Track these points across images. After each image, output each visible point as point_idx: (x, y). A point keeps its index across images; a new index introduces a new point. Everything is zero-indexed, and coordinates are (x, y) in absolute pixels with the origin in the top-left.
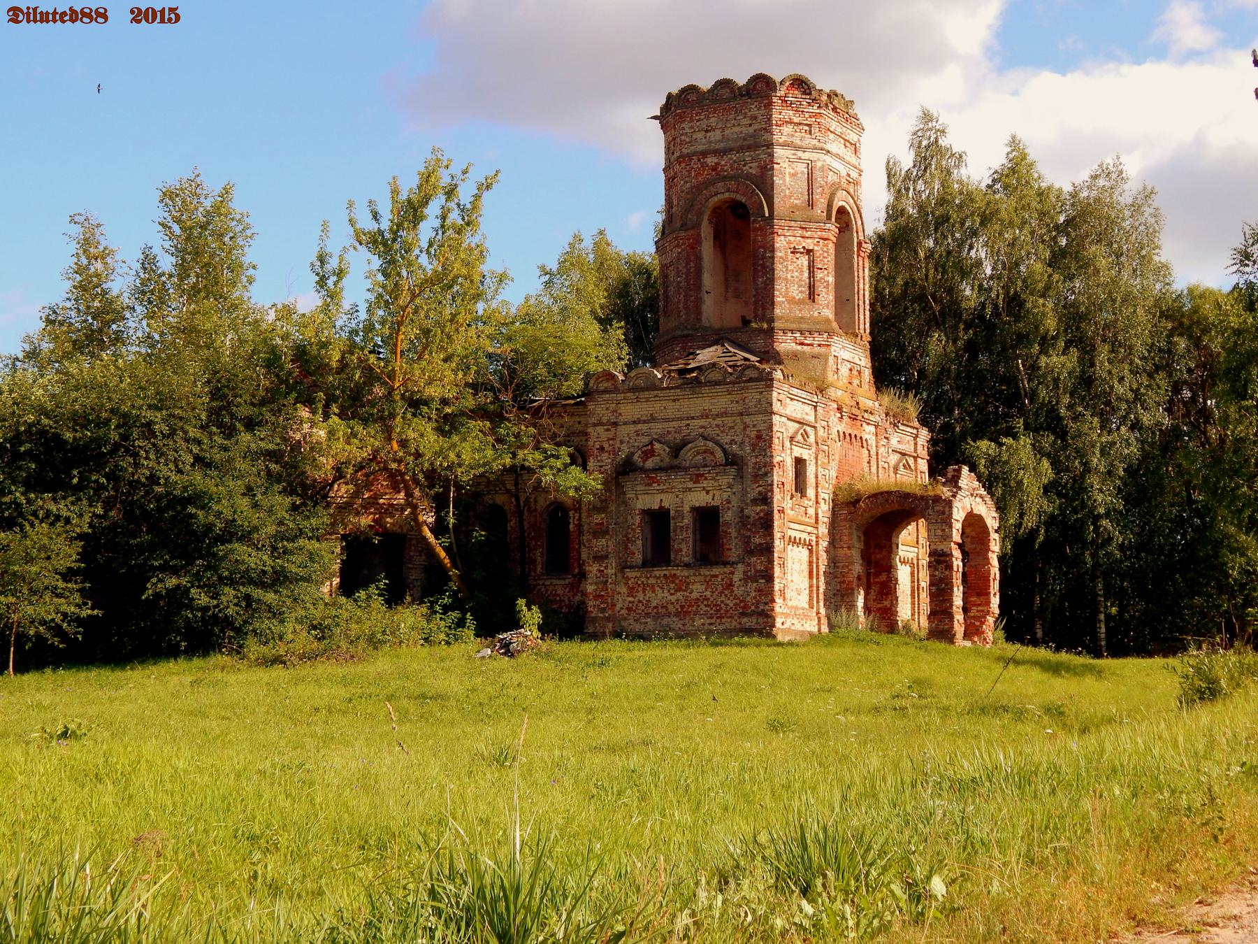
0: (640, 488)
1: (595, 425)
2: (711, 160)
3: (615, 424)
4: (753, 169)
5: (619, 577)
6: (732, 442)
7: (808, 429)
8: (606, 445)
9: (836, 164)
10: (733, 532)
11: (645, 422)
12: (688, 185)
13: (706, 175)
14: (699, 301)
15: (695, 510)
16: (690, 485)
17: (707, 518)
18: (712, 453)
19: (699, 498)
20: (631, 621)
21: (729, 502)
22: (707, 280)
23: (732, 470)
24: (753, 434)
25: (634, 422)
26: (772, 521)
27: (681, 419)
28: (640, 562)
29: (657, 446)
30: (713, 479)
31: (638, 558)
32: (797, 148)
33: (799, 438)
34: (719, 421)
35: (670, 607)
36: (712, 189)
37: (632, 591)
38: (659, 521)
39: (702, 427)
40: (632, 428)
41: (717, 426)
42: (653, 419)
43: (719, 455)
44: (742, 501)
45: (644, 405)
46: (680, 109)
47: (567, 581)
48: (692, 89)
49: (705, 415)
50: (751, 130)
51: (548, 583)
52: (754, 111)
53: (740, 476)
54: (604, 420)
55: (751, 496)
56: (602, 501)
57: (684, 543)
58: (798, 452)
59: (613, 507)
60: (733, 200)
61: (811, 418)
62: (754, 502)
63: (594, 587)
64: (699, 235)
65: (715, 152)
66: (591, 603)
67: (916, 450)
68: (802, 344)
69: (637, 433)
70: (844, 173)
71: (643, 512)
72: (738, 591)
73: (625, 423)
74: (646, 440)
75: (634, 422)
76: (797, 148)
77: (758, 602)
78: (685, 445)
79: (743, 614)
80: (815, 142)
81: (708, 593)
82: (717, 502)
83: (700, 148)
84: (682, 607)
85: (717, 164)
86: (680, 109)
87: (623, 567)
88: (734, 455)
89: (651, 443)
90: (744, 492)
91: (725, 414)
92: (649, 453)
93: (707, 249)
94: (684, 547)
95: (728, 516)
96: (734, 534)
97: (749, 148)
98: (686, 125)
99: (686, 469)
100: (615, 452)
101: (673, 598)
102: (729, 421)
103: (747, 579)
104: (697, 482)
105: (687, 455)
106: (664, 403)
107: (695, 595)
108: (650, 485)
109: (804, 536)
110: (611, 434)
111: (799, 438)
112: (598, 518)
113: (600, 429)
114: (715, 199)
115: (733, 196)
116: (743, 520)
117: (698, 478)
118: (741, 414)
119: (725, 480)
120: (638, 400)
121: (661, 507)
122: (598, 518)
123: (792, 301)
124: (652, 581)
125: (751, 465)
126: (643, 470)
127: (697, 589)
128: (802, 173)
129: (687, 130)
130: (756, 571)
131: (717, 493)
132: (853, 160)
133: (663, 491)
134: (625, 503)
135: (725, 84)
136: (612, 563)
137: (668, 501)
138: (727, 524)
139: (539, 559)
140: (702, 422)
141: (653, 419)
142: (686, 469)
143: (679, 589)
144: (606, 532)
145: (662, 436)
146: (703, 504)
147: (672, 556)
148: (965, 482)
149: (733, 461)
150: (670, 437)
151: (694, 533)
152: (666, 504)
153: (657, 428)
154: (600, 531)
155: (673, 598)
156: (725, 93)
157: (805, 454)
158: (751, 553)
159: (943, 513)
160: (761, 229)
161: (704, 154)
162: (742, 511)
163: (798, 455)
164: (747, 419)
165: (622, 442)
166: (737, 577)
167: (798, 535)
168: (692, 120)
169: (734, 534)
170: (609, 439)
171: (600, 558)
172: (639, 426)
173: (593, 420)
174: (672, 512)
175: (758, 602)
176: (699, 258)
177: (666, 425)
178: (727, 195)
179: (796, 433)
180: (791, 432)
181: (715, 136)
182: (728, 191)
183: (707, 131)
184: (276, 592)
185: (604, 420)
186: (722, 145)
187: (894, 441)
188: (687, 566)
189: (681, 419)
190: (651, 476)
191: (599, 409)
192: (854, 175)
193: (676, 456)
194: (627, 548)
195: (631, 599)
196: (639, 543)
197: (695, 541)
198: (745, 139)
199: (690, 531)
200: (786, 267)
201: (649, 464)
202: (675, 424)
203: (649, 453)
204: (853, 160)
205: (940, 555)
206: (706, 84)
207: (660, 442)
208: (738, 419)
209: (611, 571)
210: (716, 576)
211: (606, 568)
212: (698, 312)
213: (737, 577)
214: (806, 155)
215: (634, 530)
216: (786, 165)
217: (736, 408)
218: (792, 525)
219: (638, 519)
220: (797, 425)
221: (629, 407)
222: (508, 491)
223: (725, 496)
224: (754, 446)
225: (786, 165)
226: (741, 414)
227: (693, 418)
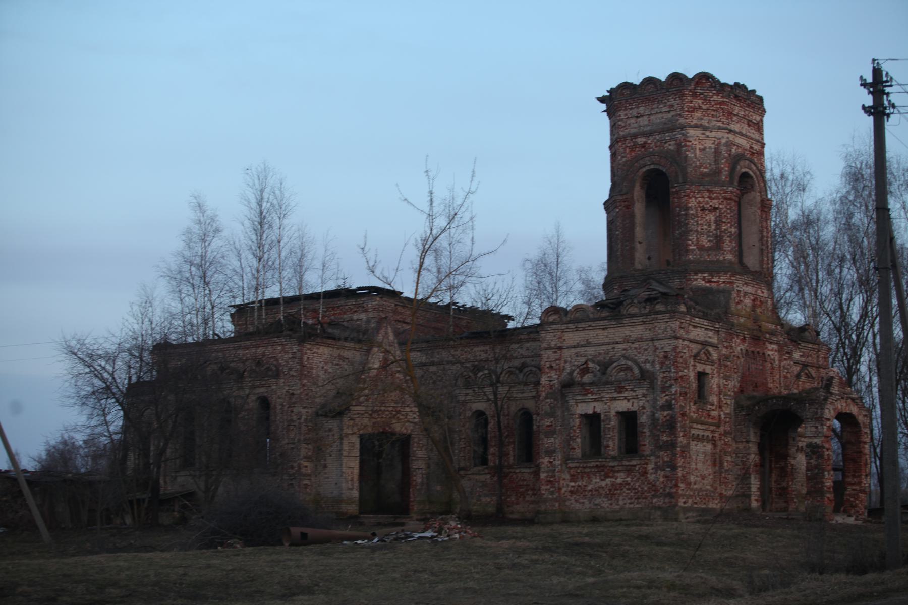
1: (546, 349)
2: (641, 140)
3: (560, 348)
5: (564, 467)
6: (646, 361)
7: (710, 349)
8: (554, 365)
9: (741, 141)
11: (582, 346)
12: (624, 160)
13: (638, 151)
14: (632, 249)
15: (619, 414)
16: (615, 395)
17: (629, 419)
19: (623, 406)
20: (573, 501)
21: (644, 408)
22: (639, 232)
23: (646, 384)
24: (661, 355)
25: (574, 347)
27: (609, 344)
28: (580, 455)
31: (578, 452)
32: (705, 128)
34: (636, 345)
35: (601, 491)
36: (641, 162)
37: (573, 478)
38: (593, 421)
39: (624, 350)
40: (573, 351)
41: (635, 348)
42: (588, 344)
43: (636, 371)
44: (654, 407)
45: (582, 333)
46: (619, 100)
48: (625, 86)
49: (626, 340)
50: (669, 116)
51: (517, 471)
52: (672, 102)
53: (652, 387)
54: (553, 345)
56: (551, 408)
57: (612, 443)
58: (700, 367)
59: (559, 413)
60: (657, 170)
61: (715, 341)
62: (663, 408)
63: (545, 475)
64: (632, 197)
66: (543, 487)
67: (818, 361)
68: (710, 282)
70: (748, 146)
71: (582, 416)
72: (651, 478)
73: (568, 348)
74: (583, 360)
75: (574, 347)
76: (705, 128)
77: (665, 486)
80: (720, 124)
81: (629, 479)
83: (633, 131)
84: (610, 490)
85: (645, 143)
87: (567, 459)
89: (586, 363)
92: (585, 370)
93: (639, 209)
94: (611, 443)
95: (643, 419)
98: (622, 113)
99: (611, 383)
101: (603, 484)
102: (644, 345)
103: (657, 468)
104: (620, 392)
105: (614, 373)
106: (596, 332)
107: (619, 481)
108: (586, 395)
109: (706, 433)
110: (557, 356)
112: (547, 422)
113: (550, 352)
114: (644, 170)
116: (654, 420)
117: (620, 389)
118: (652, 340)
119: (640, 392)
121: (595, 413)
122: (547, 422)
123: (701, 248)
124: (588, 470)
125: (660, 379)
126: (582, 385)
127: (620, 478)
128: (710, 148)
129: (623, 117)
131: (635, 401)
133: (595, 400)
134: (568, 409)
135: (650, 81)
137: (599, 408)
138: (643, 425)
139: (511, 453)
140: (625, 346)
141: (588, 344)
142: (611, 383)
143: (607, 476)
146: (625, 410)
149: (645, 376)
150: (601, 358)
152: (598, 410)
153: (591, 351)
154: (551, 433)
155: (603, 484)
156: (651, 88)
157: (708, 369)
158: (660, 448)
159: (816, 413)
161: (635, 136)
163: (700, 370)
164: (657, 343)
165: (566, 362)
166: (650, 467)
167: (701, 433)
168: (626, 110)
169: (648, 433)
170: (557, 360)
171: (550, 453)
172: (578, 350)
173: (544, 345)
174: (602, 417)
175: (665, 486)
176: (632, 216)
177: (598, 348)
178: (652, 167)
179: (701, 350)
180: (695, 351)
181: (644, 121)
183: (637, 117)
186: (649, 128)
187: (797, 355)
188: (614, 458)
189: (609, 344)
190: (585, 389)
192: (756, 147)
193: (604, 373)
195: (573, 484)
196: (579, 440)
198: (665, 123)
199: (616, 431)
200: (697, 222)
201: (587, 378)
203: (585, 370)
204: (756, 136)
206: (636, 79)
207: (593, 362)
209: (558, 463)
210: (635, 466)
211: (554, 460)
212: (632, 259)
213: (650, 467)
214: (713, 134)
215: (575, 431)
216: (696, 142)
217: (648, 335)
219: (577, 421)
220: (700, 347)
221: (571, 334)
222: (489, 400)
223: (641, 403)
224: (662, 364)
225: (696, 142)
226: (652, 340)
227: (617, 343)
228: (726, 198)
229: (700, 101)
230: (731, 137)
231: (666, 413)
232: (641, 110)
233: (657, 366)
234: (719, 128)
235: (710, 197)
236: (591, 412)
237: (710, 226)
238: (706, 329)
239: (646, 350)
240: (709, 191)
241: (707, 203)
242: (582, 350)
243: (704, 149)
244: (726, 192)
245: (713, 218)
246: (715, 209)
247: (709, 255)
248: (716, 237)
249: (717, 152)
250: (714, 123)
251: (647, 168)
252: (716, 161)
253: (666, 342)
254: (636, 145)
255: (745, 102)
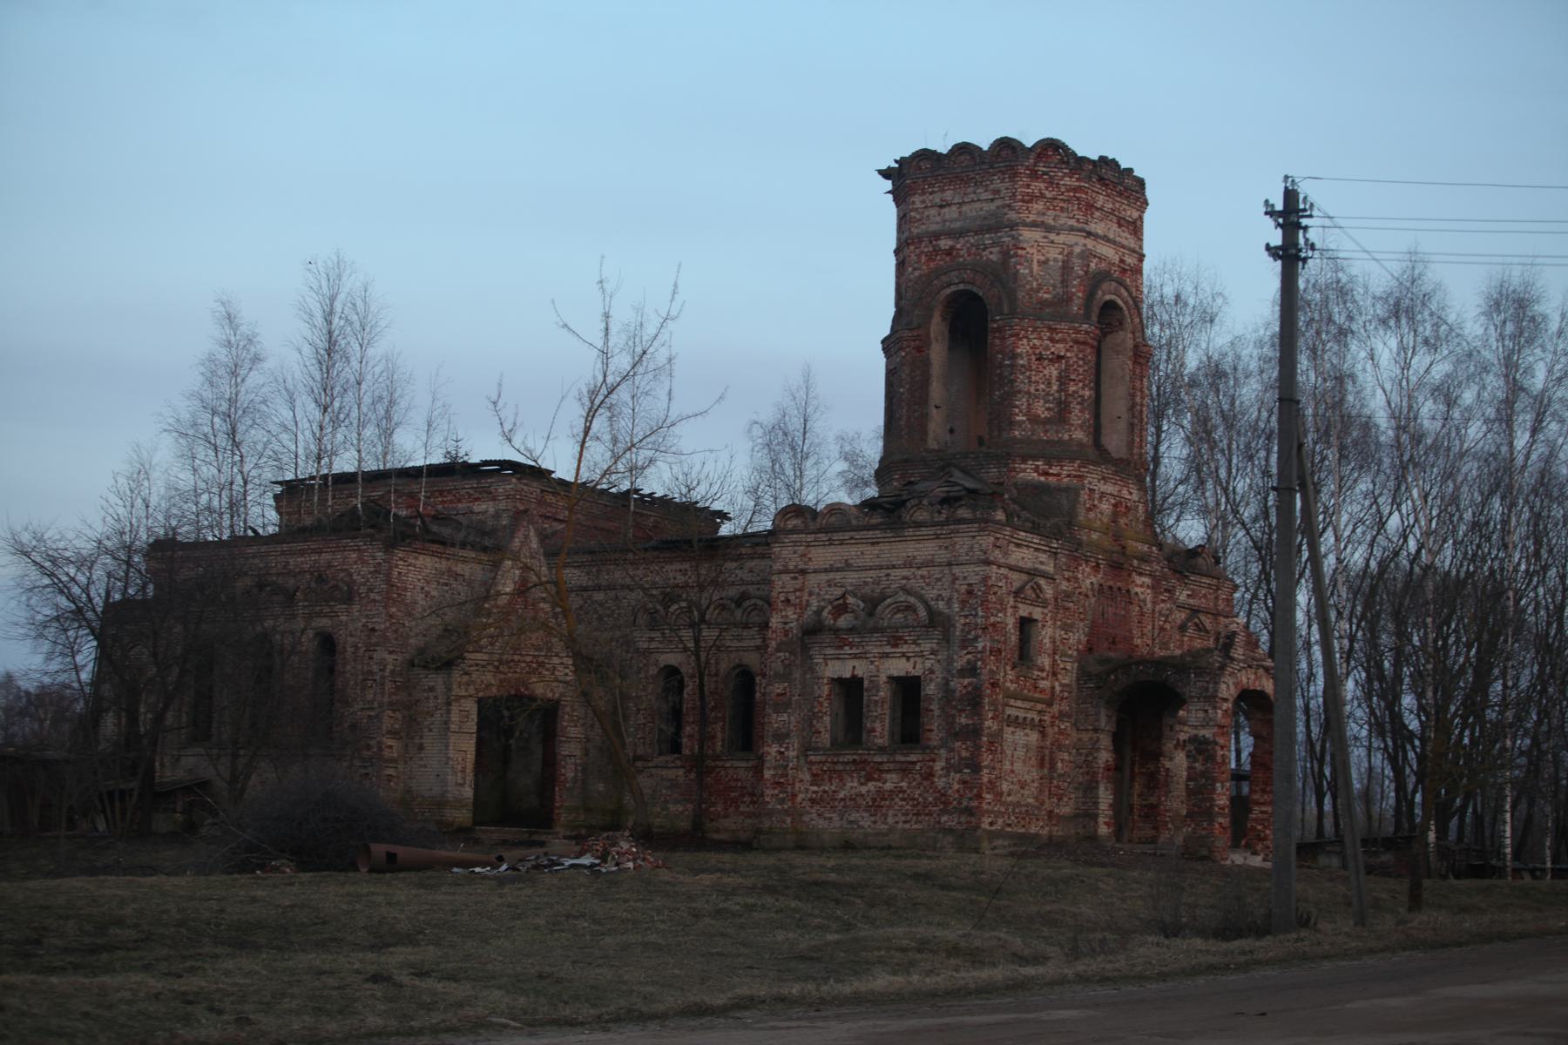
0: (830, 651)
1: (780, 572)
2: (945, 243)
3: (803, 572)
4: (993, 255)
5: (802, 761)
7: (1042, 582)
8: (792, 598)
10: (935, 707)
11: (838, 570)
12: (917, 273)
13: (940, 261)
14: (924, 418)
16: (888, 649)
17: (908, 688)
18: (915, 611)
21: (932, 672)
22: (936, 390)
24: (963, 589)
25: (826, 571)
26: (981, 697)
29: (851, 600)
30: (914, 642)
31: (825, 739)
32: (1049, 229)
33: (1029, 592)
34: (924, 572)
37: (816, 779)
38: (851, 689)
39: (905, 578)
40: (824, 577)
42: (847, 566)
43: (922, 613)
44: (949, 671)
45: (839, 549)
46: (913, 177)
47: (750, 764)
49: (908, 564)
50: (993, 206)
51: (728, 764)
52: (997, 184)
53: (946, 639)
54: (791, 566)
55: (958, 665)
56: (785, 667)
57: (880, 724)
58: (1024, 611)
59: (797, 675)
60: (970, 292)
61: (1050, 568)
62: (962, 673)
65: (951, 234)
66: (768, 792)
68: (1046, 474)
69: (830, 583)
70: (1116, 259)
72: (940, 783)
73: (815, 572)
74: (839, 592)
75: (826, 571)
76: (1049, 229)
78: (885, 599)
79: (944, 812)
81: (904, 784)
82: (918, 672)
83: (933, 227)
84: (874, 800)
85: (952, 248)
86: (913, 177)
87: (806, 749)
88: (941, 614)
89: (843, 596)
90: (950, 660)
91: (929, 563)
92: (841, 608)
94: (877, 725)
95: (930, 689)
96: (937, 713)
97: (990, 229)
99: (881, 630)
100: (803, 607)
101: (864, 789)
103: (949, 768)
105: (886, 617)
106: (862, 548)
107: (888, 786)
108: (841, 647)
111: (1029, 592)
114: (948, 291)
115: (969, 287)
117: (896, 641)
120: (831, 543)
122: (778, 688)
123: (1034, 420)
124: (839, 767)
125: (959, 626)
126: (836, 631)
128: (1055, 260)
129: (918, 205)
130: (961, 759)
131: (919, 660)
132: (1131, 243)
133: (855, 657)
134: (812, 670)
136: (795, 742)
137: (862, 668)
138: (930, 699)
139: (719, 735)
140: (905, 572)
141: (847, 566)
142: (881, 630)
143: (869, 778)
144: (788, 705)
145: (857, 586)
146: (903, 674)
147: (864, 736)
148: (1240, 651)
150: (867, 590)
151: (893, 709)
152: (859, 673)
153: (851, 578)
154: (782, 705)
155: (864, 789)
157: (1037, 613)
158: (956, 736)
160: (999, 330)
161: (937, 236)
162: (947, 683)
163: (1025, 614)
164: (956, 570)
165: (811, 594)
166: (939, 766)
167: (1021, 714)
168: (923, 193)
169: (937, 713)
171: (781, 737)
172: (832, 575)
173: (778, 566)
176: (927, 363)
177: (864, 574)
178: (962, 287)
180: (1016, 585)
181: (951, 213)
182: (963, 282)
183: (941, 207)
184: (1325, 556)
185: (791, 566)
186: (957, 225)
188: (882, 750)
189: (881, 568)
190: (841, 638)
191: (786, 553)
194: (811, 726)
196: (827, 719)
197: (893, 720)
199: (886, 706)
201: (844, 621)
202: (872, 573)
203: (841, 608)
204: (1131, 243)
205: (1201, 743)
206: (984, 140)
207: (855, 596)
208: (946, 571)
209: (792, 754)
210: (914, 763)
213: (939, 766)
214: (1061, 239)
215: (821, 704)
217: (943, 556)
218: (1012, 702)
219: (826, 689)
220: (1025, 577)
221: (820, 550)
223: (928, 664)
224: (963, 603)
226: (950, 564)
227: (894, 567)
228: (1076, 342)
229: (1042, 185)
230: (1090, 243)
231: (966, 681)
232: (948, 195)
233: (956, 607)
234: (1072, 229)
235: (1051, 340)
236: (848, 675)
237: (1049, 384)
238: (1037, 550)
239: (939, 580)
240: (1050, 329)
241: (1047, 348)
242: (838, 576)
243: (1046, 262)
244: (1078, 332)
245: (1055, 373)
246: (1060, 358)
247: (1046, 432)
248: (1059, 403)
249: (1066, 267)
250: (1064, 220)
251: (954, 288)
252: (1065, 282)
253: (972, 568)
254: (936, 250)
255: (1117, 187)
